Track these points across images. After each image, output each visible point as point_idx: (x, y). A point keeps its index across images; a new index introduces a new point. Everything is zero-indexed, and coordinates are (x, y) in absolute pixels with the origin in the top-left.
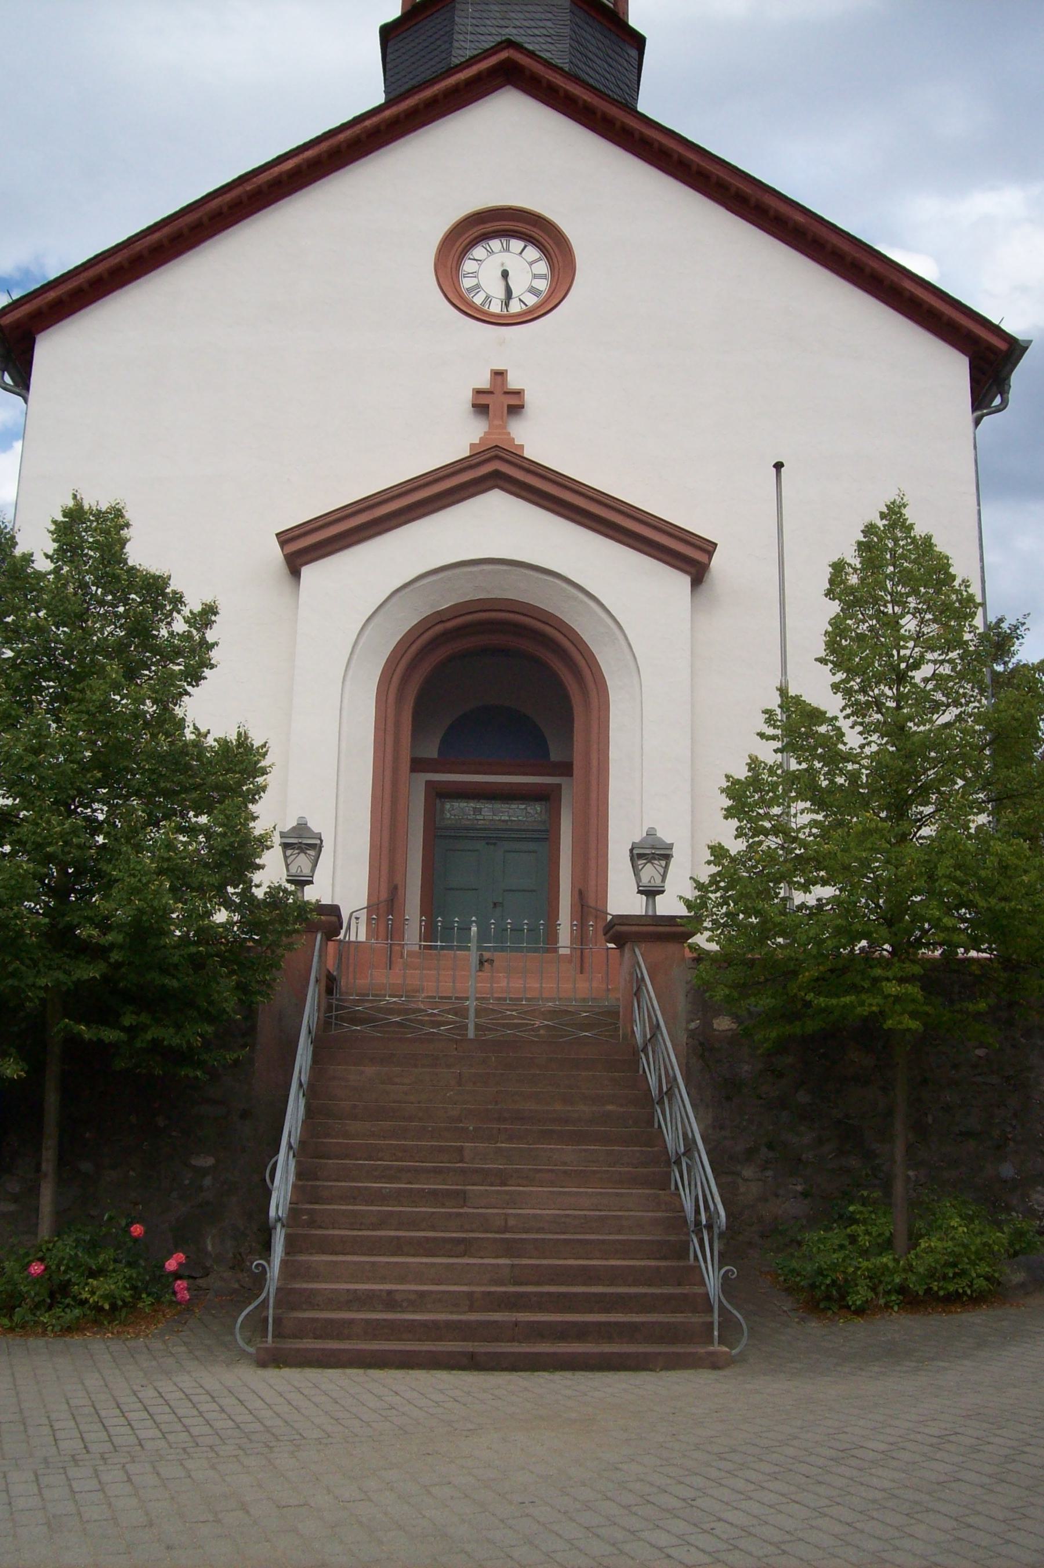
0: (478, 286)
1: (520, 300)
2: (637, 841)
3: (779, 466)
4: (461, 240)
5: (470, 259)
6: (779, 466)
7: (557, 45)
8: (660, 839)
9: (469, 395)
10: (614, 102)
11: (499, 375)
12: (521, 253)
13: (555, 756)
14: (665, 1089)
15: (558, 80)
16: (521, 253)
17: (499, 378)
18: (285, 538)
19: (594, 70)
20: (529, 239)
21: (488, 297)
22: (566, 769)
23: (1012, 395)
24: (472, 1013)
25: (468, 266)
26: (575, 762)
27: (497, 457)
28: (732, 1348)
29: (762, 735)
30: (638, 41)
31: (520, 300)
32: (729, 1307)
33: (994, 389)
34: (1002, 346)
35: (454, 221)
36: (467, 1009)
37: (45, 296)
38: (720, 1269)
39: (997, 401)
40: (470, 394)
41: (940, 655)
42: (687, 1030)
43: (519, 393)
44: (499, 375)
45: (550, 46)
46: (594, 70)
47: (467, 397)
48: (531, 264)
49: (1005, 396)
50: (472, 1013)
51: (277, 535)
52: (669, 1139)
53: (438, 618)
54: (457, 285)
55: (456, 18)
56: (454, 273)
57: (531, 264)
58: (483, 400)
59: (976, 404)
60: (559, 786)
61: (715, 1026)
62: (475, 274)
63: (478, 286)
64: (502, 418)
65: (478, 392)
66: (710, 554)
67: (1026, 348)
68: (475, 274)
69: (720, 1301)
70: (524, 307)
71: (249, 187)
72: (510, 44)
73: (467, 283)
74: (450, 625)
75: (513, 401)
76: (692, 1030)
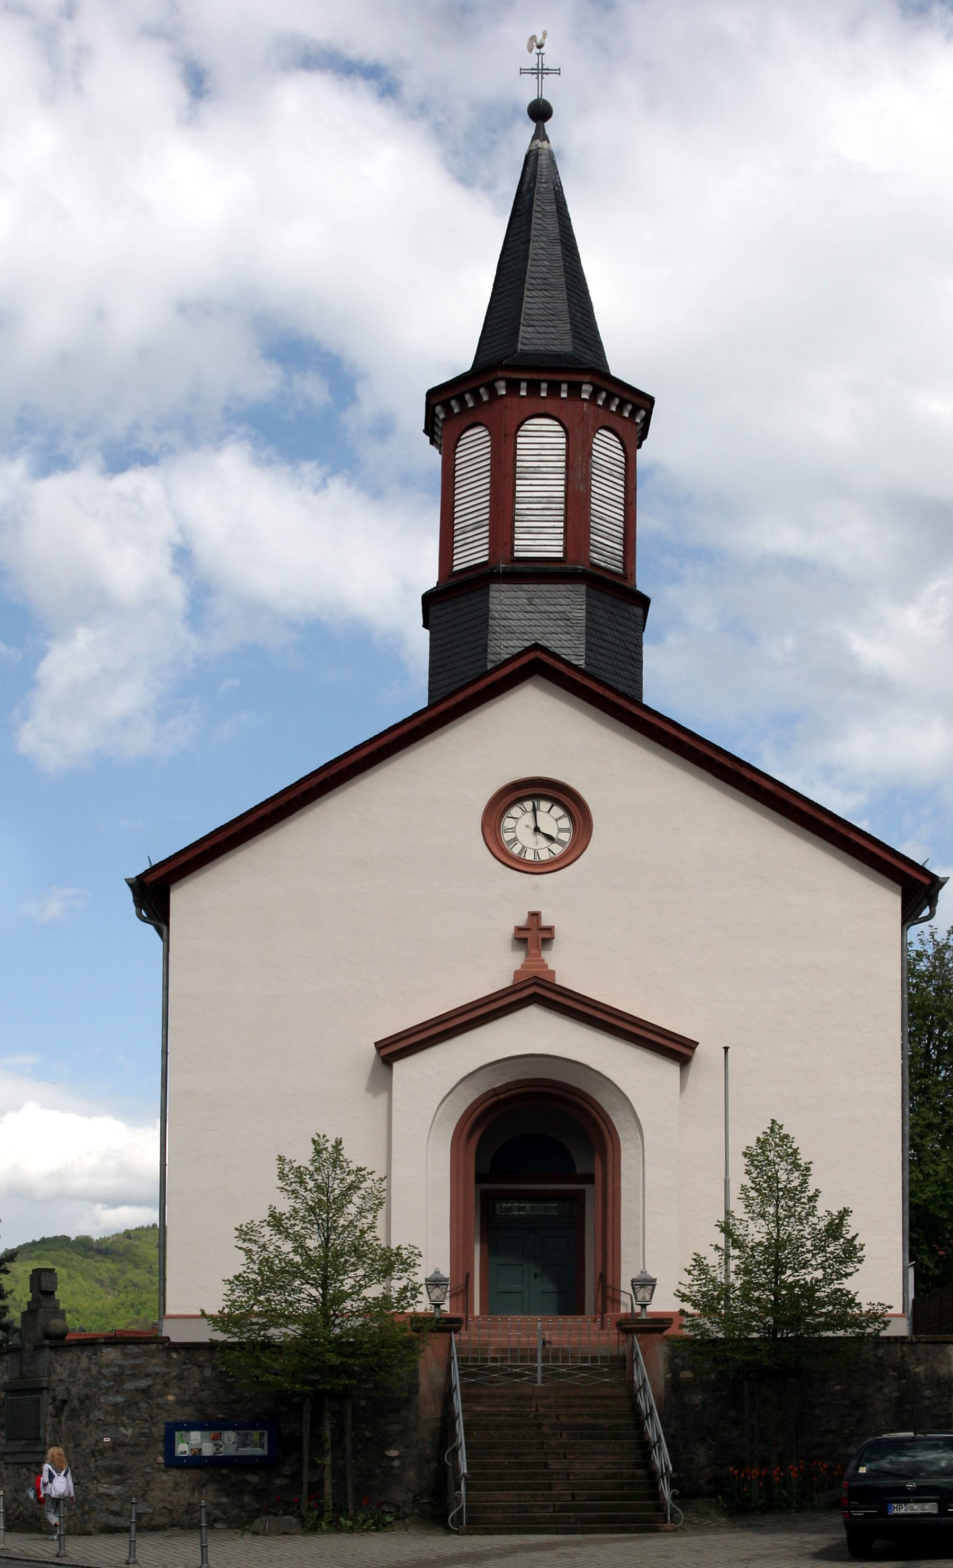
0: (515, 840)
1: (549, 849)
2: (635, 1277)
3: (726, 1049)
4: (501, 804)
5: (509, 817)
6: (726, 1049)
7: (575, 628)
8: (649, 1275)
9: (512, 930)
10: (623, 695)
11: (535, 915)
12: (549, 811)
13: (580, 1170)
14: (648, 1412)
15: (578, 678)
16: (549, 811)
17: (535, 918)
18: (380, 1046)
19: (606, 641)
20: (555, 801)
21: (524, 847)
22: (589, 1179)
23: (939, 908)
24: (539, 1370)
25: (508, 823)
26: (596, 1175)
27: (535, 984)
28: (676, 1524)
29: (675, 1294)
30: (644, 602)
31: (549, 849)
32: (675, 1507)
33: (925, 901)
34: (926, 881)
35: (498, 789)
36: (535, 1370)
37: (178, 859)
38: (670, 1491)
39: (926, 912)
40: (513, 931)
41: (690, 1331)
42: (665, 1378)
43: (550, 929)
44: (535, 915)
45: (569, 628)
46: (606, 641)
47: (509, 932)
48: (557, 820)
49: (933, 909)
50: (539, 1370)
51: (376, 1044)
52: (650, 1434)
53: (495, 1092)
54: (498, 836)
55: (490, 605)
56: (497, 823)
57: (557, 820)
58: (523, 935)
59: (904, 919)
60: (583, 1191)
61: (681, 1376)
62: (513, 830)
63: (515, 840)
64: (538, 949)
65: (519, 929)
66: (693, 1049)
67: (944, 884)
68: (513, 830)
69: (671, 1505)
70: (552, 855)
71: (333, 771)
72: (536, 647)
73: (507, 837)
74: (502, 1096)
75: (546, 935)
76: (668, 1379)
